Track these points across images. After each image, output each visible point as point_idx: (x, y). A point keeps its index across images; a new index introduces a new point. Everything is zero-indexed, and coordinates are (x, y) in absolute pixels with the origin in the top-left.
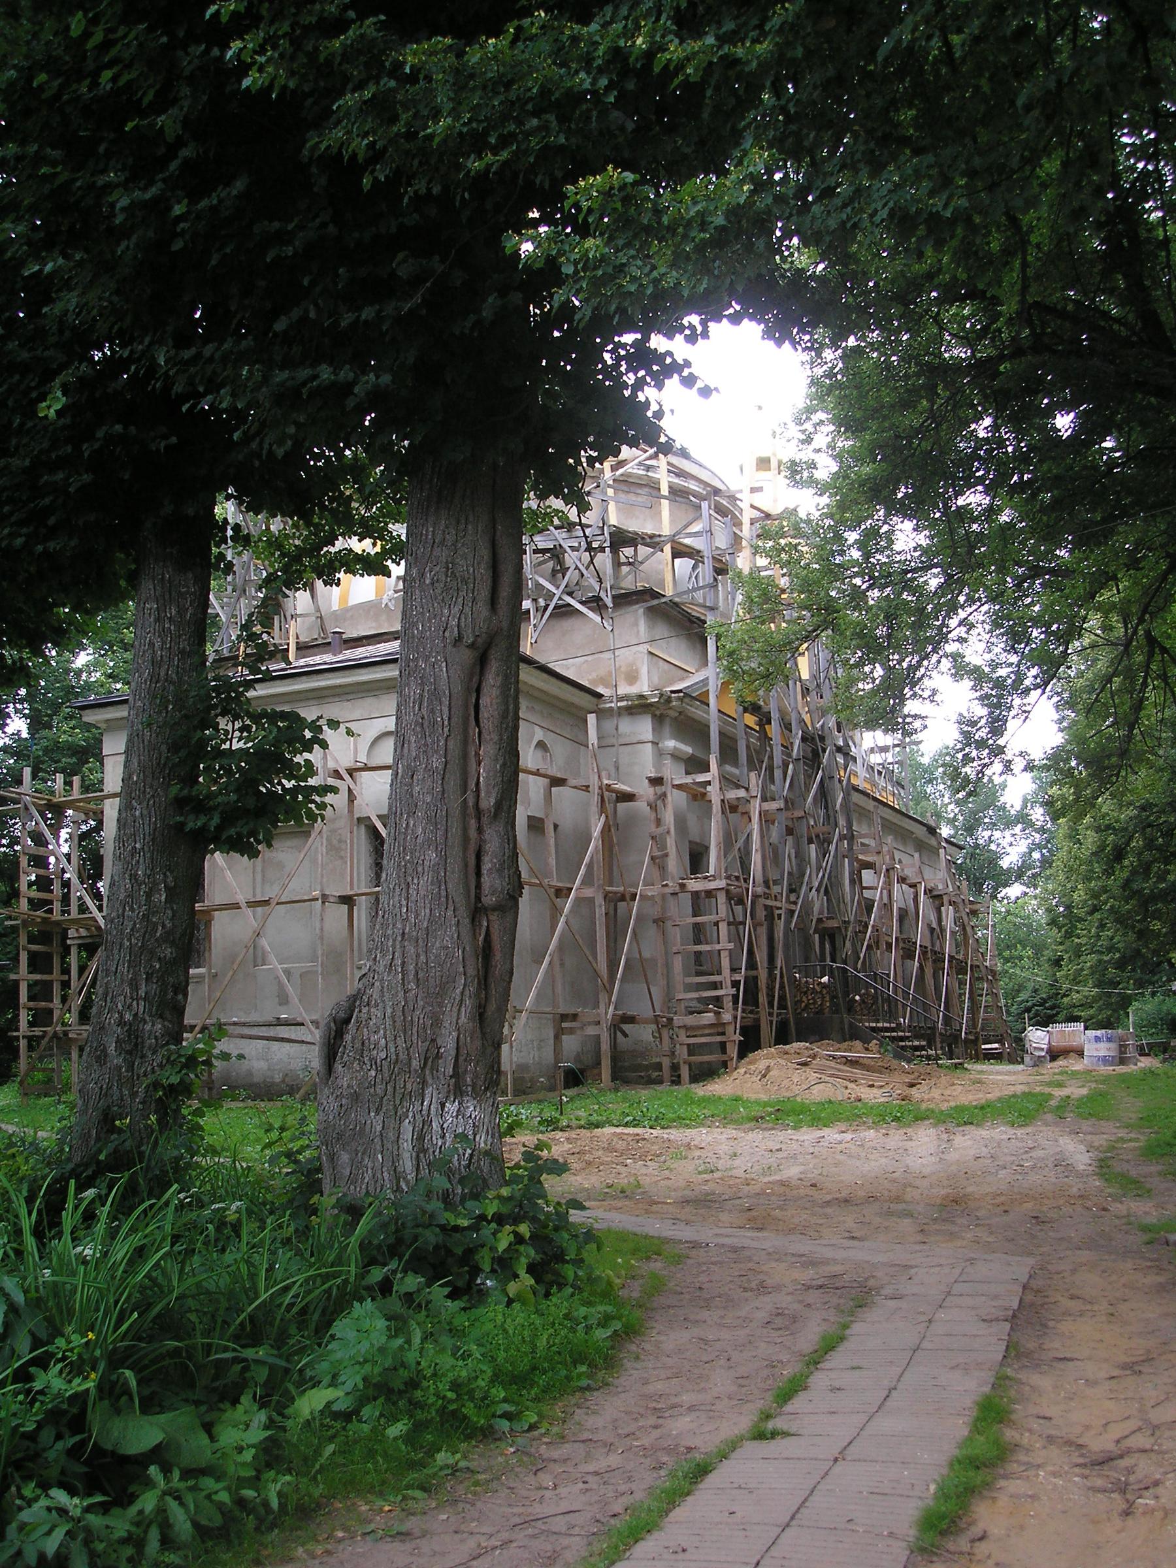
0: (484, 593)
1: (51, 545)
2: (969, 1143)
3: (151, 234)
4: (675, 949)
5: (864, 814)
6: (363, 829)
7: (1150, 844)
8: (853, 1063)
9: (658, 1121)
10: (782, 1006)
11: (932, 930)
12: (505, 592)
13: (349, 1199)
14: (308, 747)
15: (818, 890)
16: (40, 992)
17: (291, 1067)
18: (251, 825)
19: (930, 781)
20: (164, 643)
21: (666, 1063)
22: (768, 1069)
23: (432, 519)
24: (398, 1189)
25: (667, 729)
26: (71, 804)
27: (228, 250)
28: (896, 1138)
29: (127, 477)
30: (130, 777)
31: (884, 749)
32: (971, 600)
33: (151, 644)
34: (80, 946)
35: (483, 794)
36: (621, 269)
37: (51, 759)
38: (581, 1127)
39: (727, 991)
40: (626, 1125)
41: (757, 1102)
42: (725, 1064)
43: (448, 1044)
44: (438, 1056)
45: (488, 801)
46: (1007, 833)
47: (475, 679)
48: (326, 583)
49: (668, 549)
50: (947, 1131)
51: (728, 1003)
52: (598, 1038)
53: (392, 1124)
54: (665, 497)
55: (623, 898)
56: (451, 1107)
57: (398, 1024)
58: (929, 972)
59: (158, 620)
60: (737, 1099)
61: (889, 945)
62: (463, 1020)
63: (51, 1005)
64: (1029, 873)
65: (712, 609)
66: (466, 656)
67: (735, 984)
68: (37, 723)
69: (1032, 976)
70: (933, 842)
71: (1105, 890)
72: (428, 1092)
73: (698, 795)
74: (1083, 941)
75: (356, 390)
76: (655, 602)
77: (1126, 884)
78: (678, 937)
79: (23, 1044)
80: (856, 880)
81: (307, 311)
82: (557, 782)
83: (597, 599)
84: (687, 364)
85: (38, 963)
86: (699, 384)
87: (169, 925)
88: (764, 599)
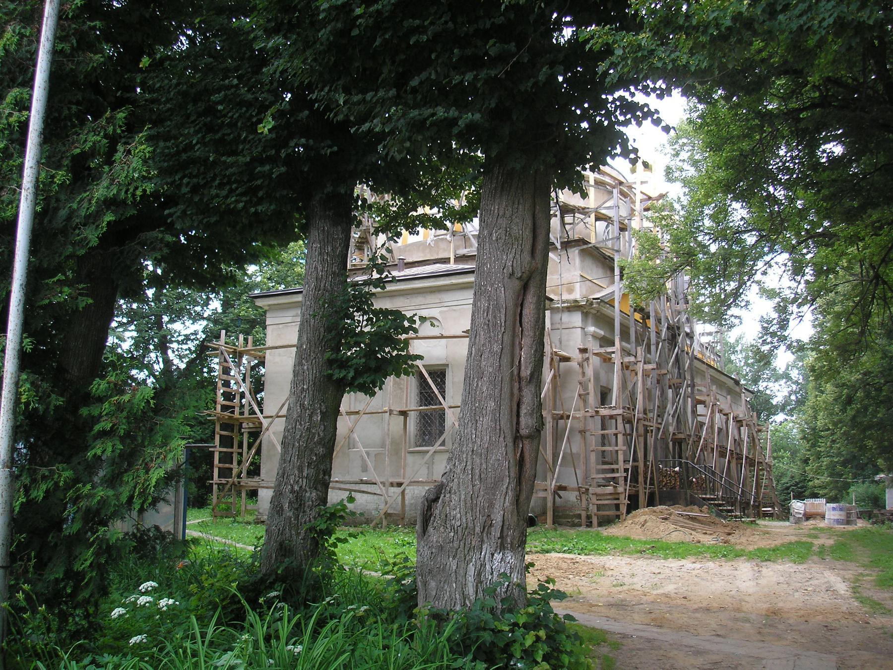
0: (528, 247)
1: (260, 208)
2: (772, 573)
3: (339, 25)
4: (591, 449)
7: (868, 395)
9: (582, 551)
10: (652, 484)
11: (735, 440)
12: (540, 246)
13: (435, 610)
14: (406, 331)
15: (673, 416)
16: (226, 458)
17: (368, 508)
18: (372, 377)
19: (733, 353)
20: (323, 267)
21: (584, 514)
22: (646, 521)
23: (497, 201)
24: (465, 604)
25: (590, 321)
26: (247, 352)
27: (387, 37)
28: (727, 568)
29: (306, 170)
30: (302, 346)
31: (710, 334)
32: (772, 250)
33: (316, 268)
34: (249, 433)
35: (523, 368)
36: (652, 52)
37: (235, 325)
38: (537, 552)
39: (620, 474)
40: (564, 552)
41: (640, 541)
42: (618, 517)
43: (497, 518)
44: (491, 525)
45: (526, 372)
46: (776, 384)
47: (521, 298)
48: (410, 233)
49: (593, 216)
50: (757, 565)
52: (545, 499)
53: (463, 565)
54: (592, 186)
55: (562, 417)
58: (733, 465)
59: (320, 254)
60: (627, 539)
61: (713, 449)
62: (507, 504)
63: (232, 466)
64: (789, 408)
65: (618, 251)
66: (517, 284)
67: (626, 470)
68: (226, 304)
69: (789, 468)
70: (737, 389)
71: (840, 421)
72: (484, 547)
73: (607, 360)
74: (822, 449)
75: (460, 123)
76: (585, 247)
77: (854, 418)
78: (593, 442)
79: (215, 487)
80: (694, 412)
81: (430, 74)
84: (657, 112)
85: (226, 442)
86: (663, 124)
87: (322, 434)
88: (650, 246)
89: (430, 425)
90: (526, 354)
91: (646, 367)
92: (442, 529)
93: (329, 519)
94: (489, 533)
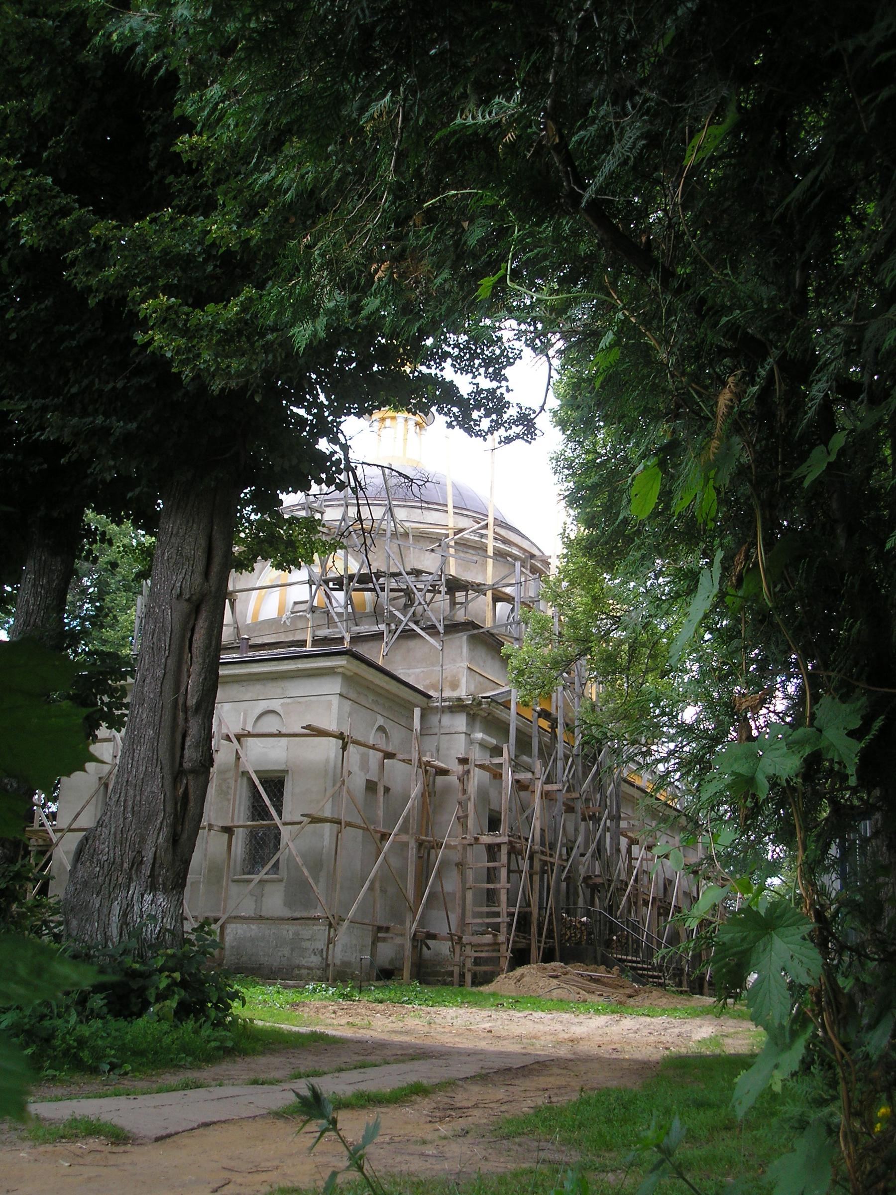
0: (200, 567)
5: (632, 801)
6: (245, 779)
8: (592, 979)
20: (36, 600)
22: (522, 976)
25: (478, 725)
39: (503, 919)
43: (148, 856)
44: (141, 862)
45: (192, 701)
49: (489, 593)
51: (503, 929)
52: (402, 946)
56: (148, 898)
57: (118, 839)
59: (33, 586)
62: (160, 840)
66: (184, 606)
67: (511, 915)
72: (133, 885)
76: (475, 632)
82: (389, 755)
83: (433, 627)
89: (261, 847)
90: (193, 682)
91: (548, 787)
92: (88, 864)
93: (12, 879)
94: (138, 870)
